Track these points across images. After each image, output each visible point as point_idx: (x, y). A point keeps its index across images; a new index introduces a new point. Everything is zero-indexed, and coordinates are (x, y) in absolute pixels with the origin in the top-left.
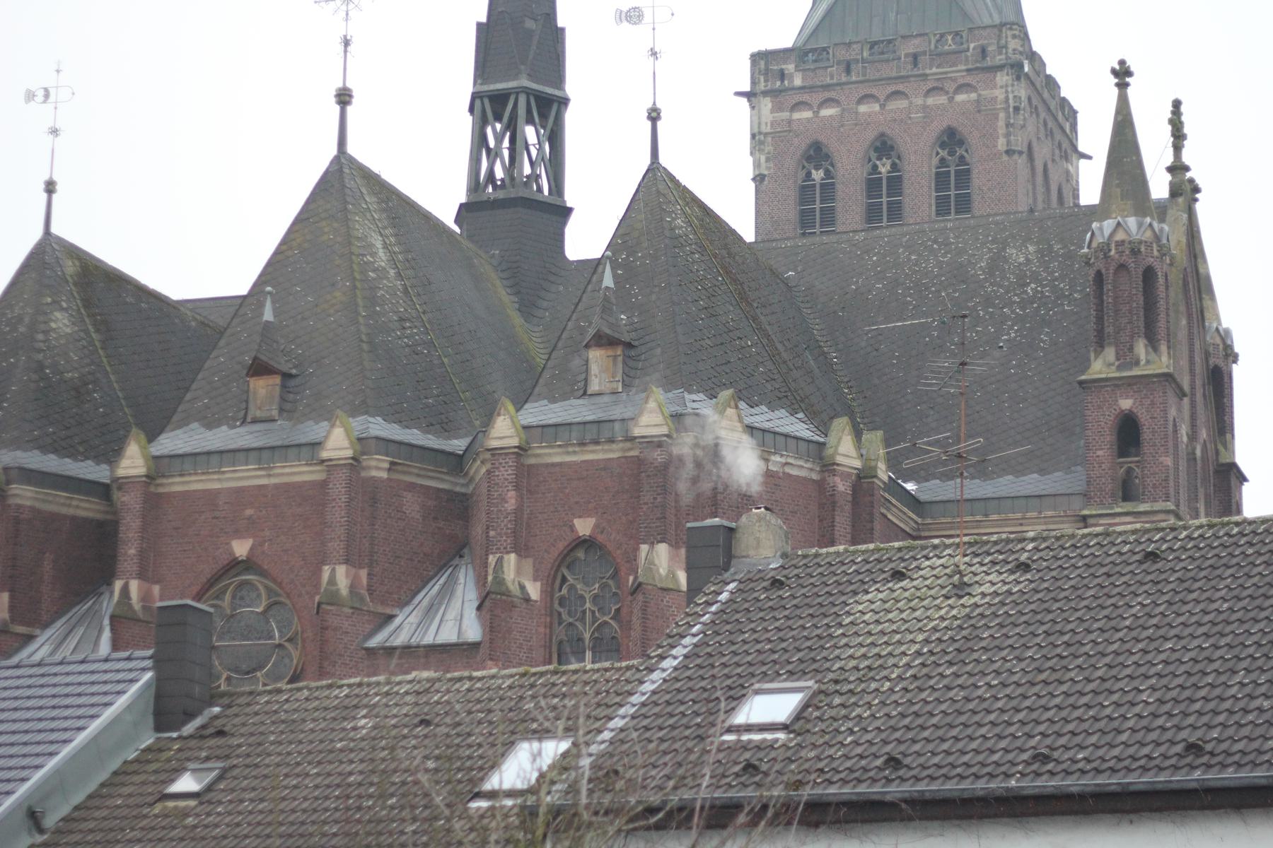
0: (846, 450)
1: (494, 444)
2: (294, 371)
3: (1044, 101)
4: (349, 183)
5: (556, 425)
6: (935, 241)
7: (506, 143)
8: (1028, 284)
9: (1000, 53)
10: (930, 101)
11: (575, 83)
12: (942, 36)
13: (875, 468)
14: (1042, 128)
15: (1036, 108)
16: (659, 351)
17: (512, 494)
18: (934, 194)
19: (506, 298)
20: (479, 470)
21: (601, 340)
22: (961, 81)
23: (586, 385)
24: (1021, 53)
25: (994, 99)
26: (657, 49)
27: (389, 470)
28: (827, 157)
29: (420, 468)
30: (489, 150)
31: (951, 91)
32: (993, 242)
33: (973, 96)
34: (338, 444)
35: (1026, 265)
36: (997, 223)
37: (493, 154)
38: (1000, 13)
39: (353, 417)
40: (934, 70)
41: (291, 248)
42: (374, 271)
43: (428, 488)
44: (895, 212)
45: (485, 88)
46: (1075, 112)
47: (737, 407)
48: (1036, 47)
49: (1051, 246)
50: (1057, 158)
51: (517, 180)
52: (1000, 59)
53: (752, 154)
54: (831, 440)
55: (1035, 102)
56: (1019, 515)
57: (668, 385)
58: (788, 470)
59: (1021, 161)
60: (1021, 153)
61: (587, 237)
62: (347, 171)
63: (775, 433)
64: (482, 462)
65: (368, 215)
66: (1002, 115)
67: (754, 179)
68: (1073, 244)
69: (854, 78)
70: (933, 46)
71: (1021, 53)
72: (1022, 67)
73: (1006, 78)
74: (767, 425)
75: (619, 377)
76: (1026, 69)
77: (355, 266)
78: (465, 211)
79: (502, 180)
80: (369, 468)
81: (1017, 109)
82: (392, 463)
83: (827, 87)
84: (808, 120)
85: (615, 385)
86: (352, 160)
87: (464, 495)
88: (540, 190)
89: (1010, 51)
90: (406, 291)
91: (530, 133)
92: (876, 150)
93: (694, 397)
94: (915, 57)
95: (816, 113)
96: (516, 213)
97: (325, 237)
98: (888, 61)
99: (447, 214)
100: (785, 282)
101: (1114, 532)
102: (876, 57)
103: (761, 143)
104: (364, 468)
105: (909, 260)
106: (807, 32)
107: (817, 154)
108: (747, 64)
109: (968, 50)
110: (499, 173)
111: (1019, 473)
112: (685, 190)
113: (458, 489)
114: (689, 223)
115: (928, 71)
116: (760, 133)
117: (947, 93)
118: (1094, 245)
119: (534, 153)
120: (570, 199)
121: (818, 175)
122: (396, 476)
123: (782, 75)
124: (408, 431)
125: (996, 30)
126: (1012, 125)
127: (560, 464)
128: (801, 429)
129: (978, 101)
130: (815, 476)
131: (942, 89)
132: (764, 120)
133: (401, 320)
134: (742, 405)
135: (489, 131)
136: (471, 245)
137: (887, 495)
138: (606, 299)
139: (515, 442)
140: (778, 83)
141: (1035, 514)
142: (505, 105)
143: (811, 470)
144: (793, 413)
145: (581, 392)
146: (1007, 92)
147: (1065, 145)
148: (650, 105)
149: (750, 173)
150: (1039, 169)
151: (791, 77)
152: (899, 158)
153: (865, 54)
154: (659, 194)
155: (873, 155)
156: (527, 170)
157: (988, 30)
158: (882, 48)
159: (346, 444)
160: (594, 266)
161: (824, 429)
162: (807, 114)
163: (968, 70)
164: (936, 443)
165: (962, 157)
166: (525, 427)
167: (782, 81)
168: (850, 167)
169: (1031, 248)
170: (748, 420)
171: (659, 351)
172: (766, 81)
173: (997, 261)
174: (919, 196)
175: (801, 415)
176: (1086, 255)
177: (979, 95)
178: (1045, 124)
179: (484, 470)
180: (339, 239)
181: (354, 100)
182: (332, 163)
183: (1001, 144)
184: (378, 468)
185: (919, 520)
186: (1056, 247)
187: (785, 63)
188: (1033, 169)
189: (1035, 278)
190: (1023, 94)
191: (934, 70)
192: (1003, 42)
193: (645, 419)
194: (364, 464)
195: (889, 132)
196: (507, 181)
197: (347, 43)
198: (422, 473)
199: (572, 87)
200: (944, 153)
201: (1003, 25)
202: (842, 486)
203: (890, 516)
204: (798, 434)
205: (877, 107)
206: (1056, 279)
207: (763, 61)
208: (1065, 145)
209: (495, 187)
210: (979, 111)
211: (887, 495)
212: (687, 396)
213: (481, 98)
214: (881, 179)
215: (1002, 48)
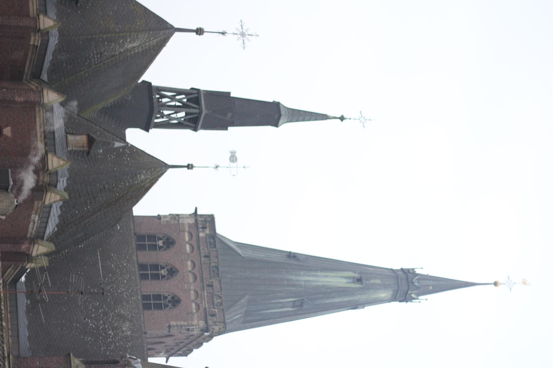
0: (39, 249)
1: (45, 92)
2: (79, 5)
3: (191, 342)
4: (162, 33)
6: (132, 291)
7: (178, 104)
8: (113, 331)
9: (212, 323)
10: (192, 292)
11: (203, 134)
13: (32, 262)
14: (179, 341)
15: (189, 338)
16: (86, 166)
17: (22, 100)
18: (151, 294)
19: (111, 101)
20: (33, 85)
21: (91, 141)
22: (201, 305)
23: (71, 134)
24: (213, 332)
25: (193, 320)
26: (218, 168)
27: (34, 45)
28: (168, 247)
29: (34, 59)
30: (175, 96)
31: (197, 301)
32: (132, 316)
33: (194, 311)
35: (122, 331)
36: (140, 318)
37: (173, 97)
38: (231, 323)
39: (58, 30)
40: (206, 294)
41: (133, 6)
42: (123, 42)
43: (26, 63)
44: (144, 277)
46: (186, 356)
47: (60, 200)
49: (129, 342)
50: (167, 348)
51: (162, 108)
52: (210, 322)
53: (170, 214)
54: (45, 243)
55: (191, 338)
56: (10, 327)
57: (70, 171)
58: (31, 223)
59: (166, 332)
60: (169, 332)
61: (135, 137)
62: (168, 31)
63: (48, 218)
64: (37, 87)
65: (148, 40)
66: (186, 323)
67: (159, 215)
68: (131, 351)
69: (202, 259)
70: (216, 293)
71: (213, 332)
72: (207, 331)
73: (202, 325)
74: (52, 214)
75: (74, 149)
76: (206, 334)
77: (125, 34)
78: (147, 85)
79: (161, 101)
80: (35, 36)
81: (188, 330)
82: (37, 47)
83: (199, 247)
84: (184, 239)
85: (71, 146)
86: (172, 34)
87: (22, 79)
88: (157, 118)
89: (214, 327)
90: (113, 56)
91: (182, 114)
92: (171, 269)
93: (65, 182)
94: (211, 286)
95: (187, 243)
96: (147, 107)
97: (138, 21)
98: (210, 273)
99: (146, 77)
100: (115, 225)
101: (5, 361)
102: (212, 269)
103: (175, 219)
104: (35, 34)
105: (124, 279)
106: (223, 239)
107: (169, 243)
108: (209, 213)
109: (214, 308)
110: (164, 100)
111: (29, 328)
113: (25, 76)
114: (142, 181)
115: (205, 291)
116: (179, 218)
117: (196, 299)
118: (131, 360)
119: (173, 116)
120: (153, 131)
121: (160, 243)
122: (31, 48)
123: (204, 228)
124: (51, 54)
125: (223, 321)
126: (181, 328)
127: (35, 122)
129: (192, 313)
130: (29, 235)
131: (197, 297)
132: (185, 220)
133: (101, 53)
134: (61, 203)
135: (183, 96)
136: (133, 86)
137: (19, 268)
138: (109, 143)
140: (200, 226)
141: (10, 334)
142: (195, 103)
143: (32, 234)
144: (57, 226)
145: (68, 131)
147: (172, 351)
149: (161, 214)
150: (161, 340)
151: (203, 232)
152: (168, 279)
154: (155, 169)
155: (169, 267)
156: (166, 112)
157: (223, 317)
158: (216, 271)
159: (46, 26)
160: (123, 138)
161: (50, 239)
162: (187, 239)
163: (205, 309)
164: (46, 280)
165: (167, 306)
168: (163, 257)
169: (129, 333)
170: (54, 206)
171: (86, 166)
172: (202, 221)
173: (123, 318)
174: (151, 287)
175: (56, 229)
176: (126, 356)
177: (194, 313)
178: (182, 342)
179: (33, 87)
180: (137, 27)
181: (198, 36)
182: (171, 25)
183: (173, 323)
184: (35, 40)
185: (8, 283)
186: (129, 344)
187: (209, 229)
188: (162, 337)
189: (116, 335)
190: (195, 332)
191: (206, 294)
192: (218, 324)
193: (55, 160)
194: (37, 34)
195: (179, 274)
196: (161, 104)
197: (223, 33)
198: (32, 60)
199: (202, 133)
200: (169, 298)
201: (224, 323)
202: (24, 247)
203: (10, 269)
204: (48, 228)
205: (190, 269)
206: (115, 343)
207: (210, 220)
208: (172, 351)
209: (159, 98)
210: (188, 314)
211: (19, 268)
212: (66, 178)
213: (198, 93)
214: (158, 270)
215: (215, 323)
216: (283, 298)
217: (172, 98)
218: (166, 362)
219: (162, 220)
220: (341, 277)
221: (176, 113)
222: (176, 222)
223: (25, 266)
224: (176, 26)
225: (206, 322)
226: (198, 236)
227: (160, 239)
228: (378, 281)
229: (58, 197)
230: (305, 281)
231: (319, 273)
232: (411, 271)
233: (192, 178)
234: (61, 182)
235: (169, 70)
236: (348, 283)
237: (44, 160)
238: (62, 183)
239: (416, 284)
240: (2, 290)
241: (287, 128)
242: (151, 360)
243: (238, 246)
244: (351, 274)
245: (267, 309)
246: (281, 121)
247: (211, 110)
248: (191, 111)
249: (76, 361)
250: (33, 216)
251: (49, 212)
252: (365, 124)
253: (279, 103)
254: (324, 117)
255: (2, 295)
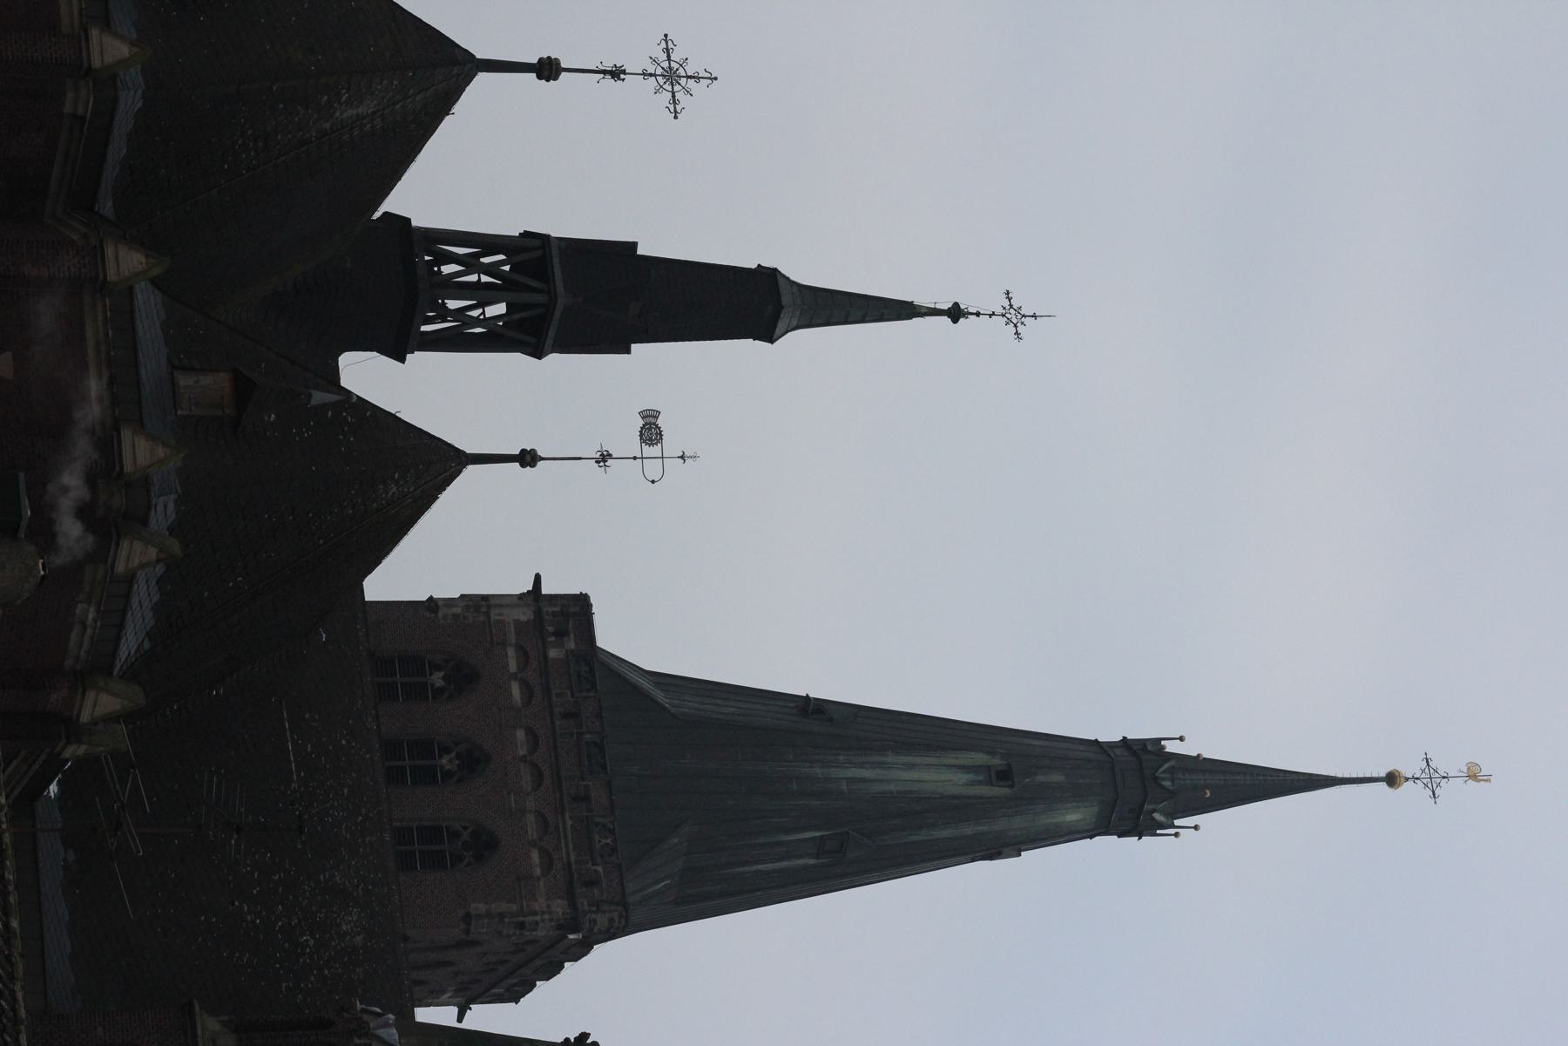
0: (101, 703)
1: (109, 251)
5: (133, 329)
10: (531, 818)
12: (612, 832)
24: (591, 930)
30: (477, 256)
33: (538, 871)
34: (109, 49)
40: (569, 823)
45: (555, 251)
47: (158, 561)
48: (599, 949)
52: (583, 903)
60: (467, 932)
61: (363, 373)
66: (514, 908)
71: (591, 930)
72: (573, 932)
74: (135, 602)
78: (400, 223)
81: (521, 926)
86: (469, 79)
93: (171, 506)
95: (514, 676)
96: (407, 289)
99: (397, 202)
101: (19, 1032)
106: (615, 664)
107: (463, 678)
110: (447, 269)
112: (432, 499)
115: (567, 815)
116: (489, 607)
118: (366, 1017)
119: (475, 313)
120: (416, 358)
121: (437, 679)
123: (561, 634)
128: (130, 644)
130: (69, 663)
135: (502, 257)
137: (43, 757)
139: (112, 276)
140: (551, 629)
146: (543, 913)
148: (539, 453)
153: (588, 736)
154: (428, 466)
156: (453, 304)
159: (109, 60)
160: (332, 376)
162: (513, 666)
163: (569, 864)
166: (131, 289)
167: (554, 634)
169: (359, 939)
170: (141, 575)
175: (147, 645)
183: (479, 907)
190: (541, 933)
200: (465, 835)
203: (15, 763)
207: (578, 609)
209: (430, 264)
211: (43, 757)
212: (173, 497)
216: (788, 831)
217: (470, 264)
218: (460, 1020)
219: (440, 614)
220: (950, 766)
221: (482, 305)
222: (482, 618)
223: (59, 754)
224: (480, 54)
225: (573, 904)
226: (546, 657)
227: (436, 667)
228: (1057, 778)
229: (152, 553)
230: (850, 780)
231: (890, 758)
232: (1149, 747)
233: (544, 495)
234: (160, 508)
235: (463, 181)
236: (971, 783)
237: (107, 443)
238: (164, 512)
239: (1167, 784)
240: (4, 826)
241: (801, 344)
242: (424, 1015)
243: (657, 684)
244: (980, 758)
245: (746, 863)
246: (781, 326)
247: (586, 296)
248: (525, 297)
249: (209, 1024)
250: (80, 608)
251: (127, 597)
252: (1021, 328)
253: (775, 270)
254: (903, 310)
255: (7, 838)
